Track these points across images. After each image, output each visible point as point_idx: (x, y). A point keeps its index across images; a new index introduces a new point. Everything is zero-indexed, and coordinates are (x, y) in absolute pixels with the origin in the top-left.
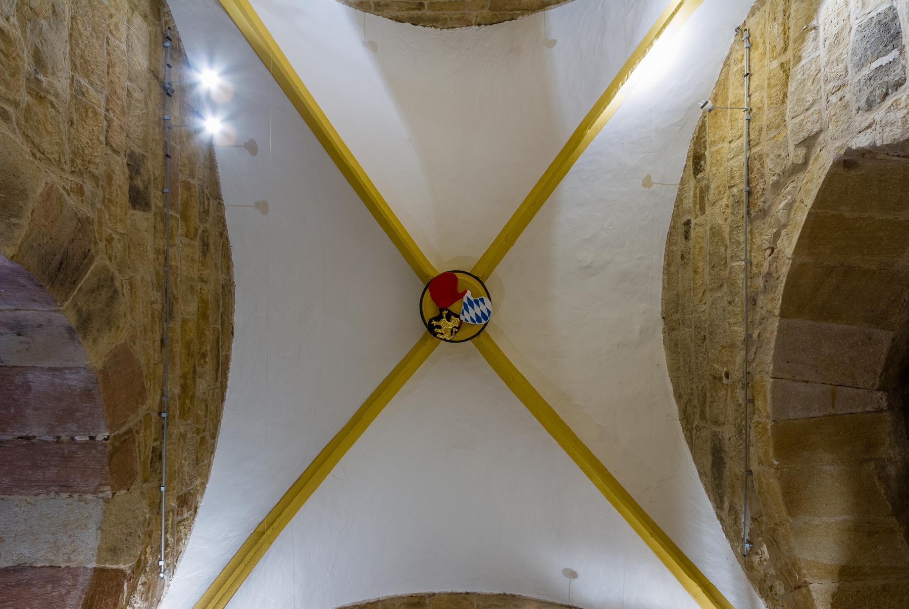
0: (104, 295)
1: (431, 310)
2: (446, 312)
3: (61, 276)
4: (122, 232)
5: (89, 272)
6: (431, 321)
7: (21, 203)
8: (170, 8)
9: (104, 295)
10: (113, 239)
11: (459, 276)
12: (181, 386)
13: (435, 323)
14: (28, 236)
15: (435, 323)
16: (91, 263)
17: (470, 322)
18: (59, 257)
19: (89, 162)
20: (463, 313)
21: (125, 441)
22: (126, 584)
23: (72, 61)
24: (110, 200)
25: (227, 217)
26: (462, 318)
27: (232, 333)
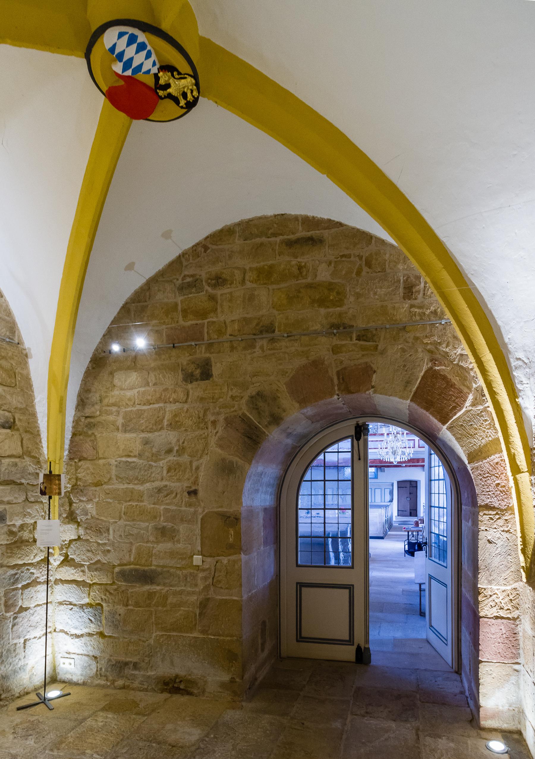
0: (261, 404)
1: (167, 107)
2: (161, 93)
3: (254, 437)
4: (226, 387)
5: (250, 416)
6: (182, 107)
7: (227, 462)
8: (93, 351)
9: (261, 404)
10: (232, 396)
11: (105, 89)
12: (319, 306)
13: (183, 102)
14: (240, 458)
15: (183, 102)
16: (246, 415)
17: (153, 57)
18: (246, 439)
19: (199, 418)
20: (148, 72)
21: (343, 379)
22: (436, 368)
23: (160, 430)
24: (213, 398)
25: (191, 245)
26: (155, 70)
27: (282, 215)
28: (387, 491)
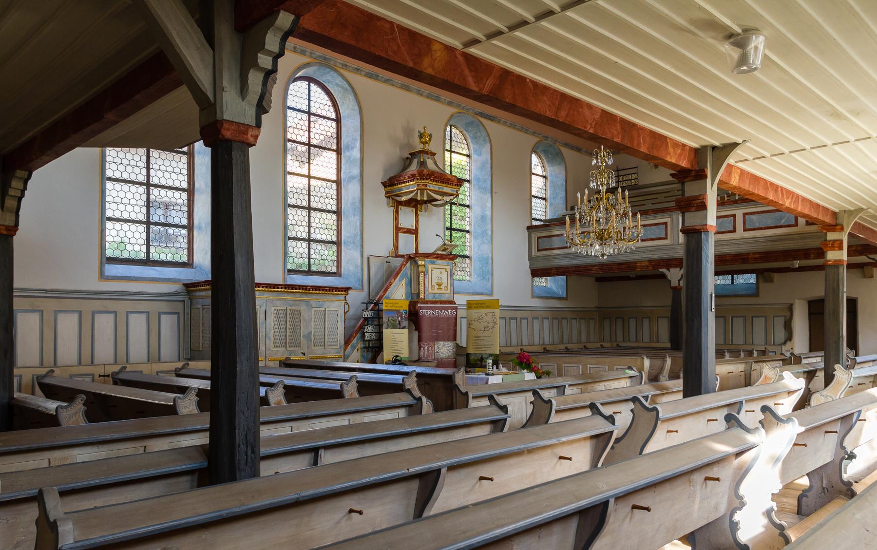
28: (780, 322)
